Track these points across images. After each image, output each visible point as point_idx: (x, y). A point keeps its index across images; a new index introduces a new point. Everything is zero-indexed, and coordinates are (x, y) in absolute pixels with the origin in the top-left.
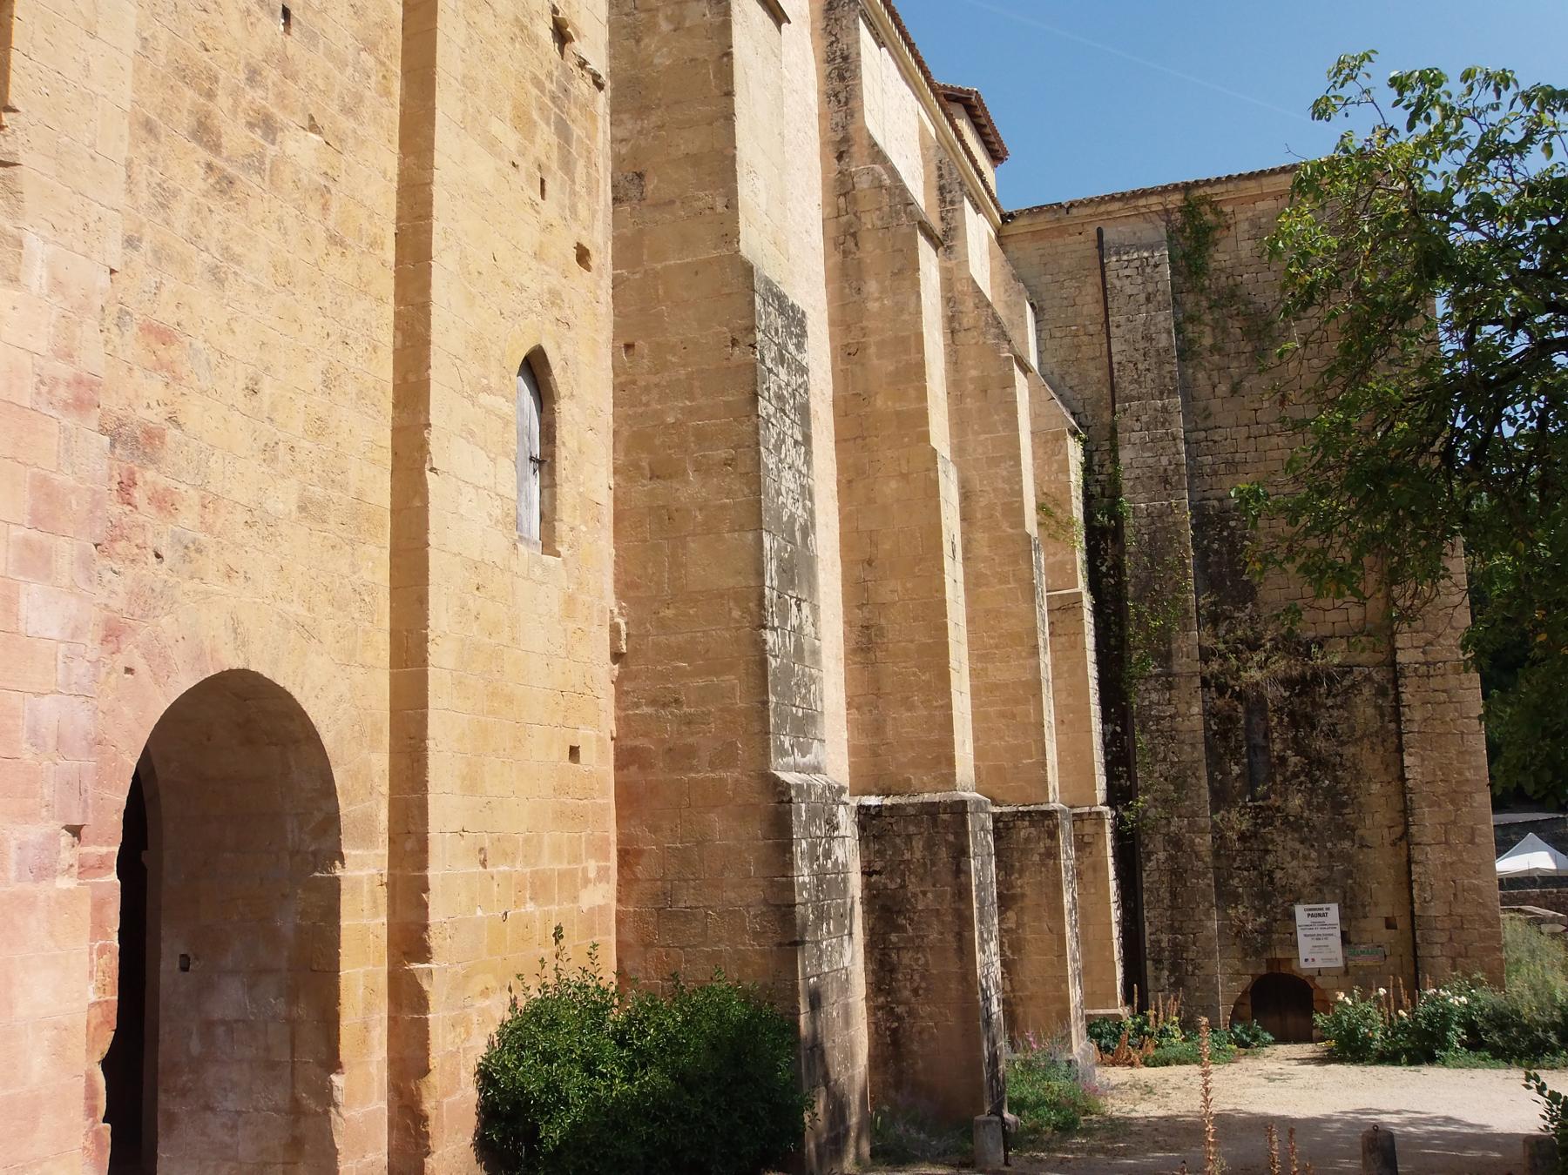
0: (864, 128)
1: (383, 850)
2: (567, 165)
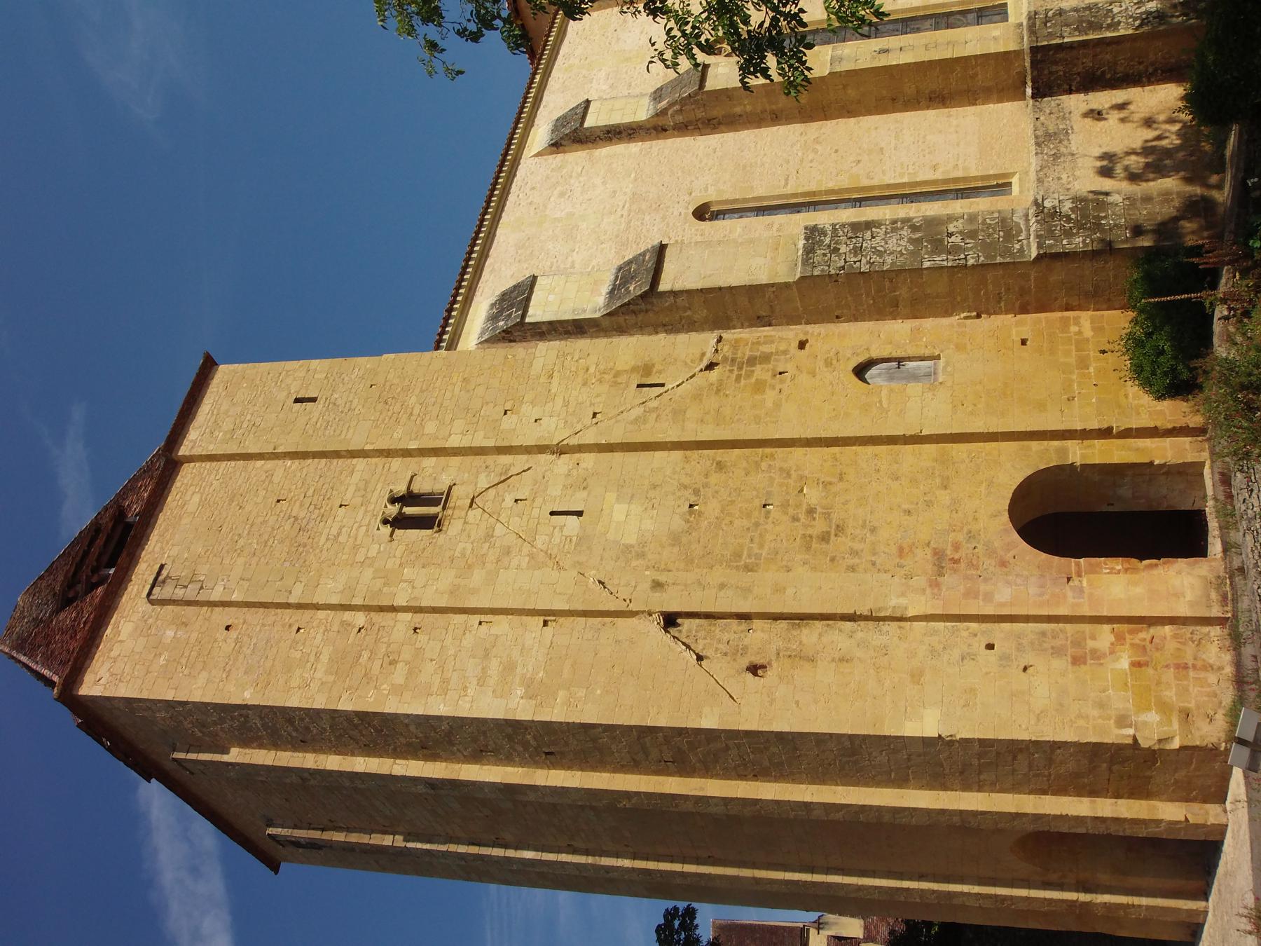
0: (647, 120)
1: (1069, 442)
2: (766, 358)
